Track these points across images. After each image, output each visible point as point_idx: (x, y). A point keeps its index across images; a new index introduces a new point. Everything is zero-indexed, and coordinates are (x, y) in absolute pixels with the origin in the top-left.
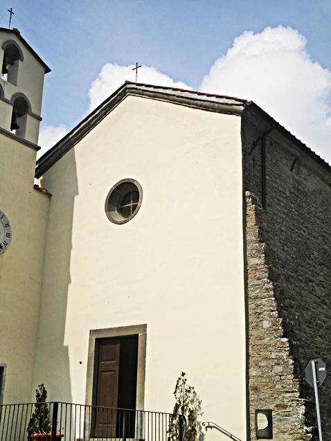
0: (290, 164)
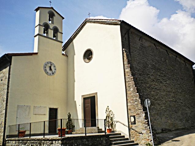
0: (139, 38)
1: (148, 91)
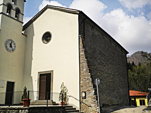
0: (91, 28)
1: (95, 72)
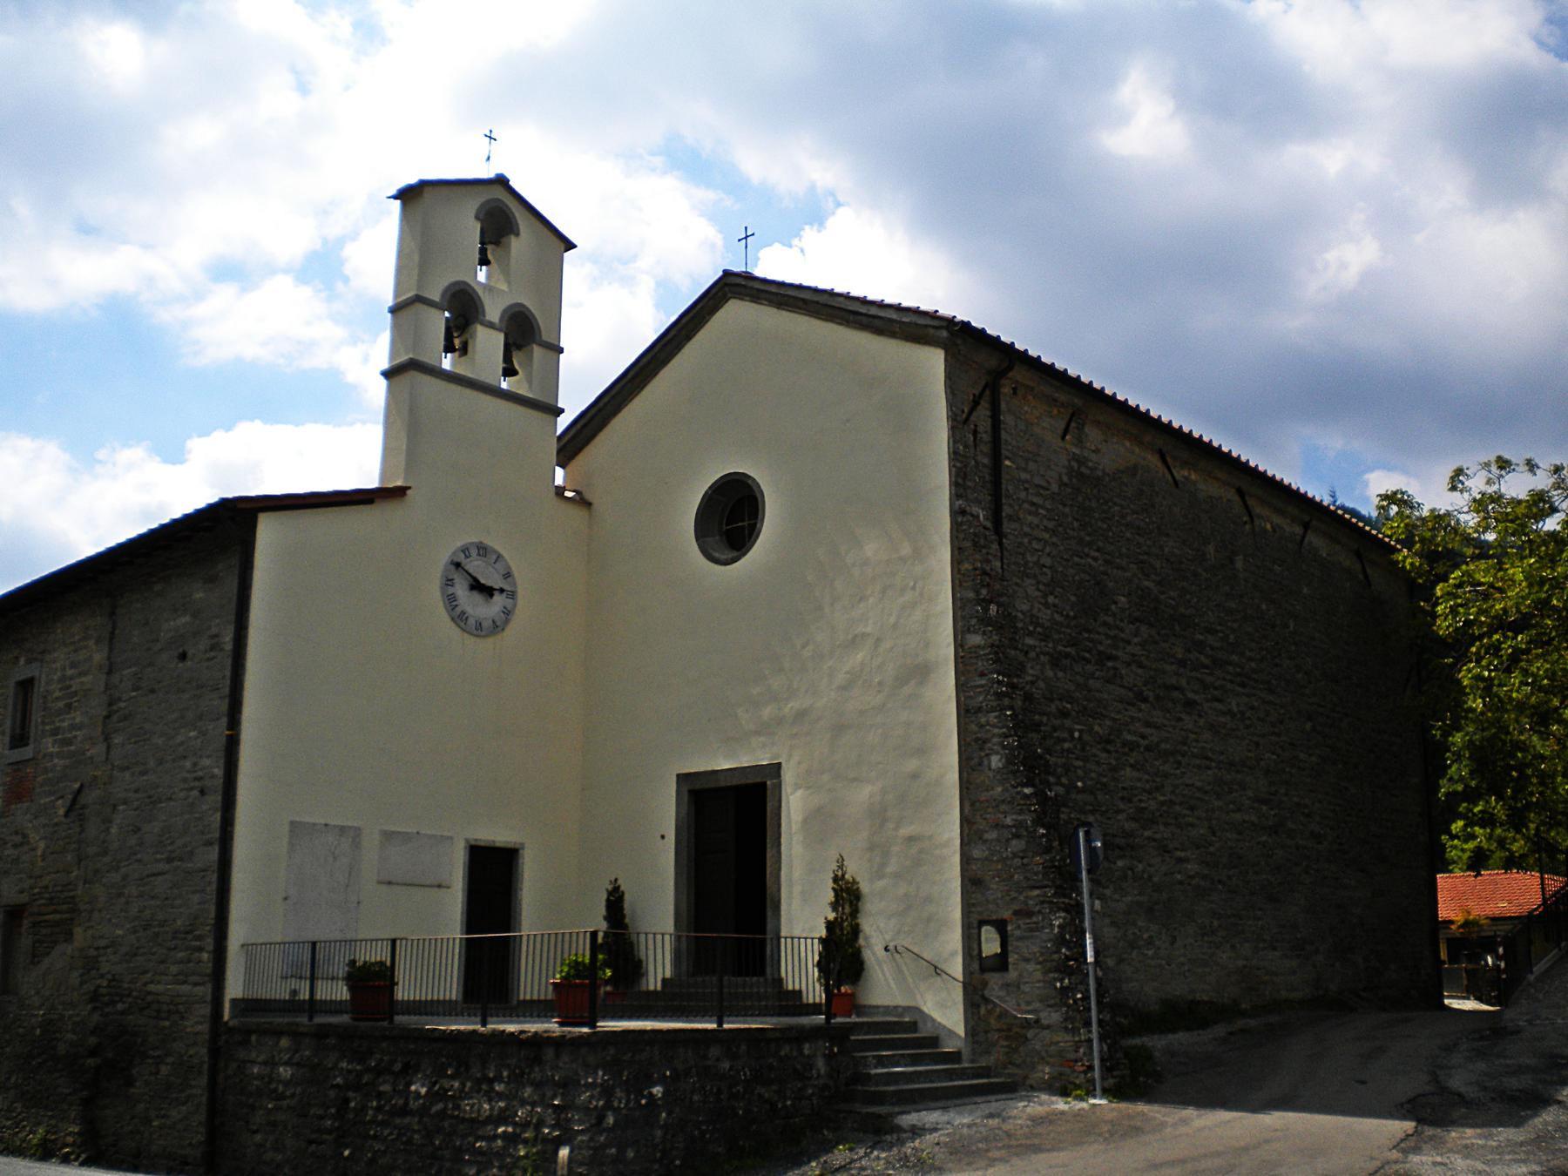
0: (1062, 425)
1: (1098, 763)
